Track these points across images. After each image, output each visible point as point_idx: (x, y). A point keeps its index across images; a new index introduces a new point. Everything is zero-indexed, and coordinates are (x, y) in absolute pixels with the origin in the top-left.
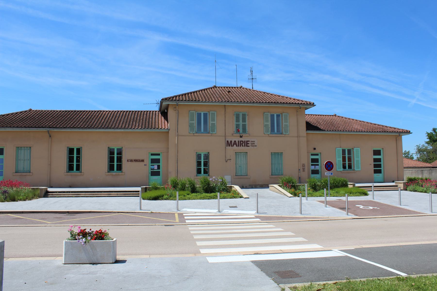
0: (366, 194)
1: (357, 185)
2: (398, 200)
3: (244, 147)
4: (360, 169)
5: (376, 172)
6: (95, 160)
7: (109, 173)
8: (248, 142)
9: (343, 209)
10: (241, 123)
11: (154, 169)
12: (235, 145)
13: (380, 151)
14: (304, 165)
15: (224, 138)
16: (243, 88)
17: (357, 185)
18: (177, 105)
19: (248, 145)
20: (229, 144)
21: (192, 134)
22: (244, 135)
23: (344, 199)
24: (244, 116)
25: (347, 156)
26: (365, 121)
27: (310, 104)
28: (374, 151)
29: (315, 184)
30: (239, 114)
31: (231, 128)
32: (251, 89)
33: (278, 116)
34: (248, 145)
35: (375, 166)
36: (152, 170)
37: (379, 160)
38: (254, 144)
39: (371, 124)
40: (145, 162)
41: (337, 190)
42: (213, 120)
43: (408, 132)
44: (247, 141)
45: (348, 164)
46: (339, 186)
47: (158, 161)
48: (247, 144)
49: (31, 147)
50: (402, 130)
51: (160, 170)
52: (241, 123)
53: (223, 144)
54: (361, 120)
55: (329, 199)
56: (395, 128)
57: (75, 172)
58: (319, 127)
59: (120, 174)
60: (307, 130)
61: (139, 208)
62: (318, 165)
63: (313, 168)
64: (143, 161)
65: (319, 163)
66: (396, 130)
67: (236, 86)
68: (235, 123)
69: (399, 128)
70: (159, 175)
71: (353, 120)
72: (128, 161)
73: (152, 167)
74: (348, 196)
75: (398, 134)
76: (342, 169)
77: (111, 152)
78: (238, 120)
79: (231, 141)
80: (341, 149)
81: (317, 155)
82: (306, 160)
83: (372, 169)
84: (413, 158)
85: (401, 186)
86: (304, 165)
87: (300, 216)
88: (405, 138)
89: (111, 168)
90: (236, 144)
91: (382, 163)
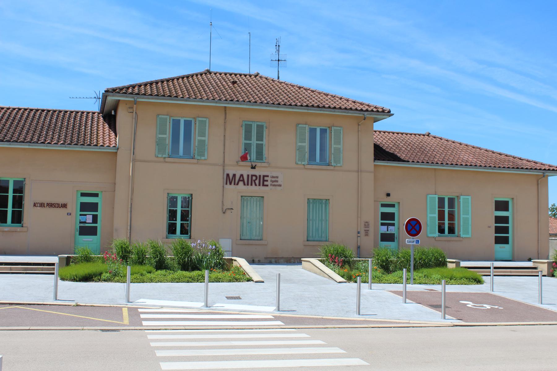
0: (479, 281)
1: (463, 264)
2: (536, 294)
3: (258, 187)
4: (469, 236)
5: (498, 241)
8: (266, 178)
9: (437, 307)
10: (254, 142)
11: (85, 222)
12: (241, 183)
14: (367, 224)
15: (221, 168)
16: (261, 77)
17: (463, 264)
18: (135, 103)
19: (266, 183)
20: (230, 180)
21: (162, 160)
22: (259, 164)
23: (438, 288)
24: (260, 128)
25: (446, 210)
26: (482, 147)
27: (383, 111)
28: (497, 202)
30: (251, 125)
31: (235, 150)
32: (276, 79)
33: (323, 131)
34: (266, 183)
35: (498, 230)
36: (82, 225)
37: (505, 220)
38: (277, 181)
40: (69, 209)
41: (426, 271)
42: (202, 134)
44: (264, 176)
45: (448, 226)
46: (430, 264)
47: (94, 207)
51: (98, 225)
52: (254, 142)
53: (220, 179)
54: (476, 145)
58: (399, 155)
59: (19, 229)
60: (375, 159)
61: (52, 295)
62: (393, 225)
63: (383, 229)
64: (64, 206)
65: (396, 222)
67: (247, 72)
68: (243, 141)
69: (544, 162)
70: (95, 234)
72: (35, 205)
73: (83, 219)
74: (447, 283)
76: (437, 234)
78: (248, 136)
79: (234, 175)
80: (437, 197)
81: (393, 206)
82: (372, 215)
83: (493, 235)
85: (544, 268)
87: (357, 317)
88: (555, 183)
90: (243, 180)
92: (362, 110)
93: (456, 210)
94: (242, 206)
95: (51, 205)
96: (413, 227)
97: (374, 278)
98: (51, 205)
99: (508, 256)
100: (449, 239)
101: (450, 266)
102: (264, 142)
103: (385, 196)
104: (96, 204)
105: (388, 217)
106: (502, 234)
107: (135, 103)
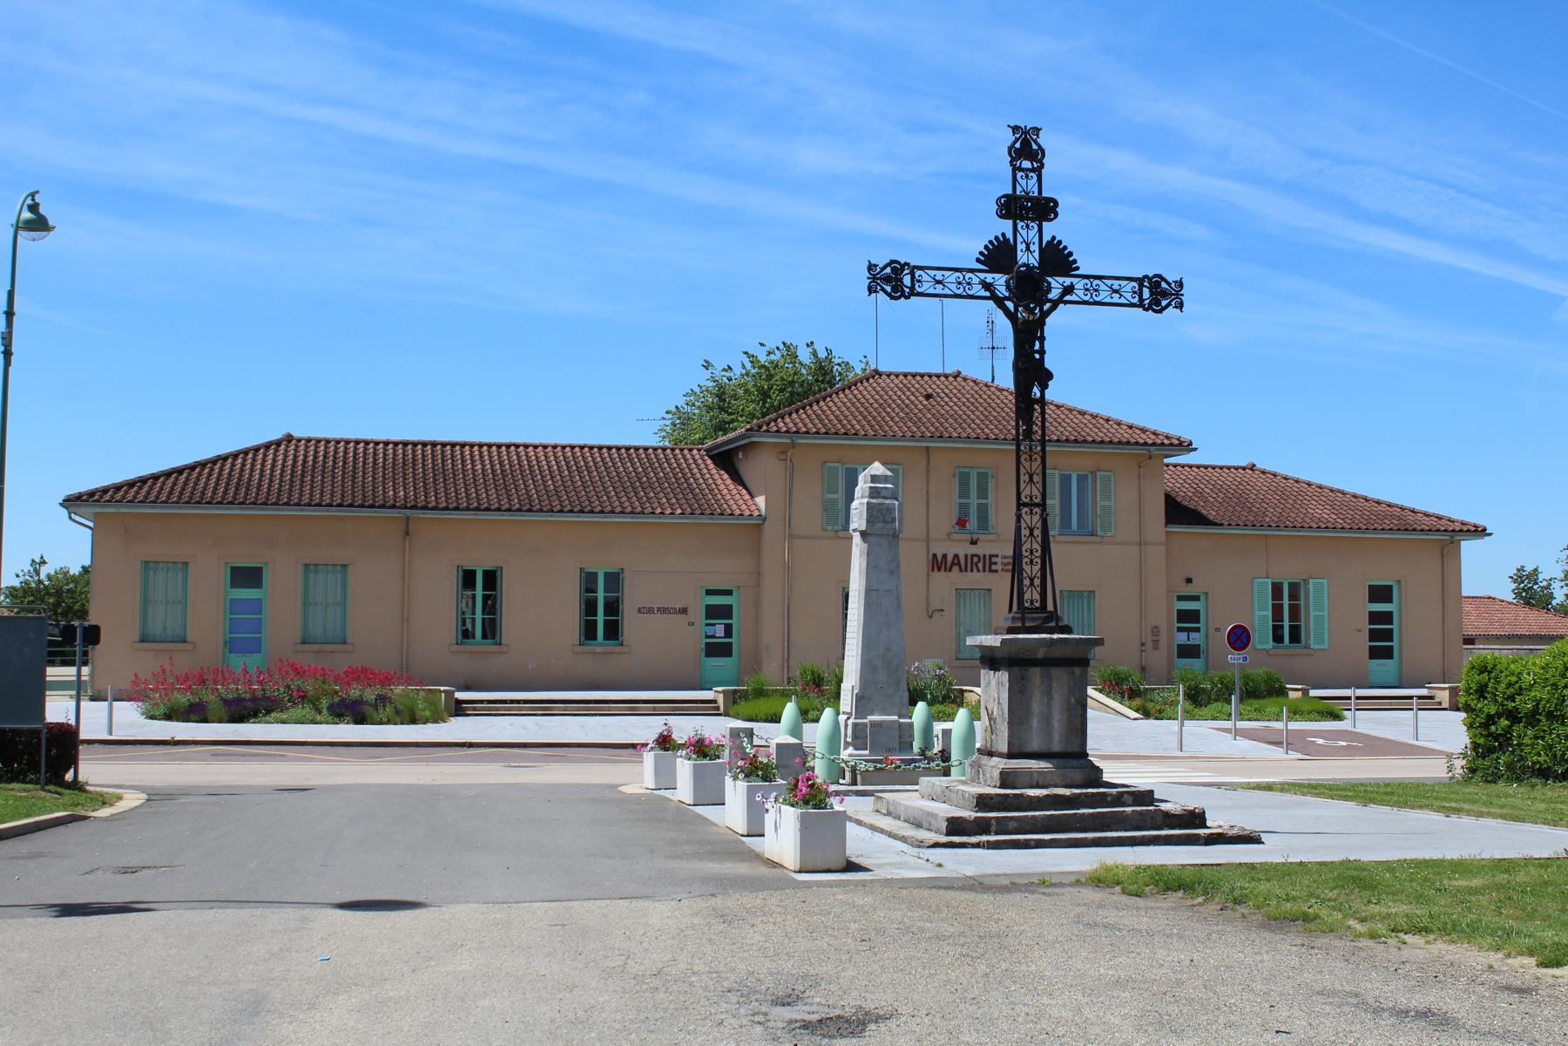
0: (1336, 717)
2: (1411, 729)
4: (1325, 646)
5: (1375, 653)
6: (541, 609)
7: (584, 648)
9: (1278, 744)
10: (974, 500)
12: (956, 568)
13: (1390, 587)
14: (1155, 631)
15: (924, 544)
16: (965, 379)
18: (793, 445)
20: (939, 564)
22: (982, 537)
26: (1347, 489)
27: (1181, 444)
29: (1196, 687)
31: (944, 519)
33: (1081, 479)
35: (1374, 635)
37: (1387, 617)
39: (1366, 500)
40: (691, 617)
41: (1256, 703)
43: (1479, 532)
45: (1289, 627)
46: (1261, 692)
47: (723, 612)
48: (991, 563)
49: (344, 566)
50: (1463, 524)
51: (734, 640)
52: (974, 500)
54: (1336, 486)
55: (1242, 724)
56: (1439, 518)
57: (478, 644)
58: (1204, 512)
59: (617, 649)
60: (1167, 523)
62: (1197, 630)
63: (1182, 638)
65: (1202, 625)
66: (1442, 525)
67: (940, 371)
68: (957, 500)
69: (1454, 516)
70: (730, 655)
71: (1309, 484)
74: (1290, 719)
75: (1447, 537)
77: (589, 582)
78: (964, 493)
79: (945, 556)
80: (1269, 581)
81: (1196, 598)
82: (1162, 613)
84: (1551, 596)
86: (1155, 631)
87: (1179, 754)
88: (1468, 547)
89: (589, 632)
91: (1395, 627)
92: (1145, 444)
93: (1302, 602)
94: (958, 604)
95: (663, 610)
96: (1238, 638)
97: (1185, 711)
98: (663, 610)
99: (1393, 680)
100: (1291, 651)
101: (1292, 695)
102: (989, 501)
103: (1183, 583)
104: (729, 607)
105: (1188, 618)
106: (1381, 642)
107: (793, 445)
